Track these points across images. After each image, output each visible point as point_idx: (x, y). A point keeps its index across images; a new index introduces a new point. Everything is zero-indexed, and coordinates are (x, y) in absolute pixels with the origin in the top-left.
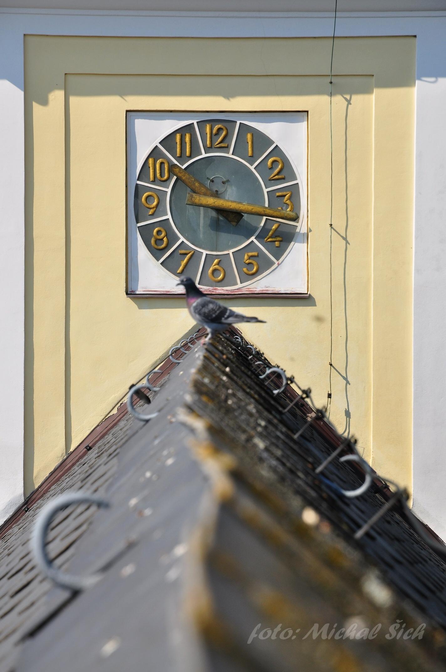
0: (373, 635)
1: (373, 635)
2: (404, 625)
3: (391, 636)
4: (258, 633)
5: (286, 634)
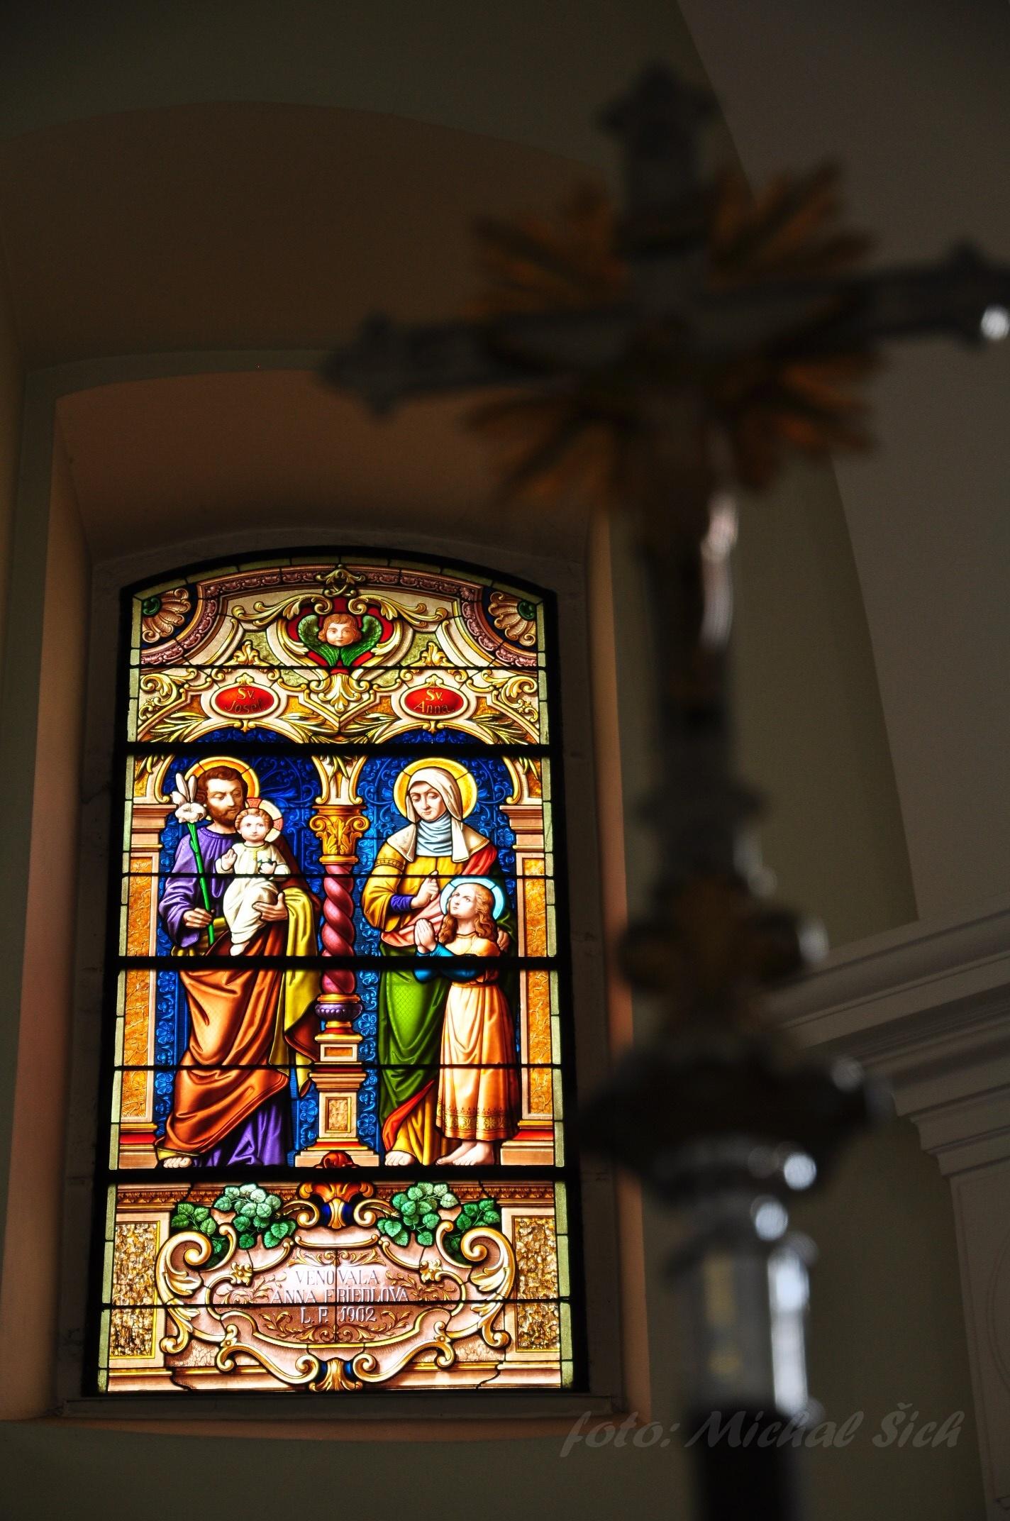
0: (845, 1438)
1: (845, 1438)
2: (916, 1415)
3: (884, 1438)
4: (584, 1432)
5: (648, 1436)
